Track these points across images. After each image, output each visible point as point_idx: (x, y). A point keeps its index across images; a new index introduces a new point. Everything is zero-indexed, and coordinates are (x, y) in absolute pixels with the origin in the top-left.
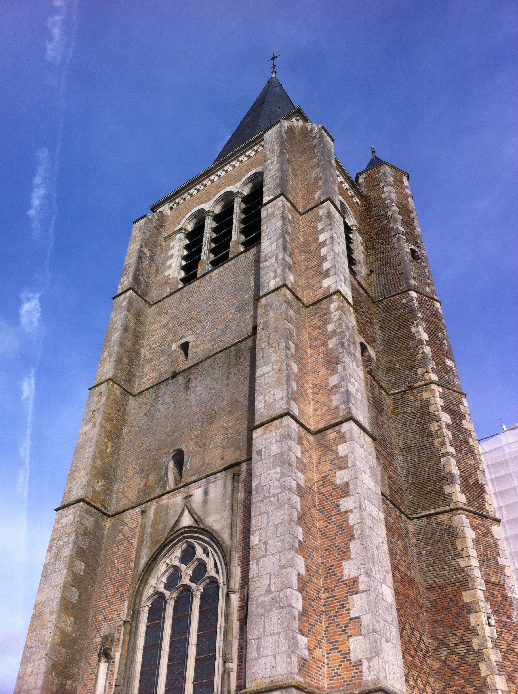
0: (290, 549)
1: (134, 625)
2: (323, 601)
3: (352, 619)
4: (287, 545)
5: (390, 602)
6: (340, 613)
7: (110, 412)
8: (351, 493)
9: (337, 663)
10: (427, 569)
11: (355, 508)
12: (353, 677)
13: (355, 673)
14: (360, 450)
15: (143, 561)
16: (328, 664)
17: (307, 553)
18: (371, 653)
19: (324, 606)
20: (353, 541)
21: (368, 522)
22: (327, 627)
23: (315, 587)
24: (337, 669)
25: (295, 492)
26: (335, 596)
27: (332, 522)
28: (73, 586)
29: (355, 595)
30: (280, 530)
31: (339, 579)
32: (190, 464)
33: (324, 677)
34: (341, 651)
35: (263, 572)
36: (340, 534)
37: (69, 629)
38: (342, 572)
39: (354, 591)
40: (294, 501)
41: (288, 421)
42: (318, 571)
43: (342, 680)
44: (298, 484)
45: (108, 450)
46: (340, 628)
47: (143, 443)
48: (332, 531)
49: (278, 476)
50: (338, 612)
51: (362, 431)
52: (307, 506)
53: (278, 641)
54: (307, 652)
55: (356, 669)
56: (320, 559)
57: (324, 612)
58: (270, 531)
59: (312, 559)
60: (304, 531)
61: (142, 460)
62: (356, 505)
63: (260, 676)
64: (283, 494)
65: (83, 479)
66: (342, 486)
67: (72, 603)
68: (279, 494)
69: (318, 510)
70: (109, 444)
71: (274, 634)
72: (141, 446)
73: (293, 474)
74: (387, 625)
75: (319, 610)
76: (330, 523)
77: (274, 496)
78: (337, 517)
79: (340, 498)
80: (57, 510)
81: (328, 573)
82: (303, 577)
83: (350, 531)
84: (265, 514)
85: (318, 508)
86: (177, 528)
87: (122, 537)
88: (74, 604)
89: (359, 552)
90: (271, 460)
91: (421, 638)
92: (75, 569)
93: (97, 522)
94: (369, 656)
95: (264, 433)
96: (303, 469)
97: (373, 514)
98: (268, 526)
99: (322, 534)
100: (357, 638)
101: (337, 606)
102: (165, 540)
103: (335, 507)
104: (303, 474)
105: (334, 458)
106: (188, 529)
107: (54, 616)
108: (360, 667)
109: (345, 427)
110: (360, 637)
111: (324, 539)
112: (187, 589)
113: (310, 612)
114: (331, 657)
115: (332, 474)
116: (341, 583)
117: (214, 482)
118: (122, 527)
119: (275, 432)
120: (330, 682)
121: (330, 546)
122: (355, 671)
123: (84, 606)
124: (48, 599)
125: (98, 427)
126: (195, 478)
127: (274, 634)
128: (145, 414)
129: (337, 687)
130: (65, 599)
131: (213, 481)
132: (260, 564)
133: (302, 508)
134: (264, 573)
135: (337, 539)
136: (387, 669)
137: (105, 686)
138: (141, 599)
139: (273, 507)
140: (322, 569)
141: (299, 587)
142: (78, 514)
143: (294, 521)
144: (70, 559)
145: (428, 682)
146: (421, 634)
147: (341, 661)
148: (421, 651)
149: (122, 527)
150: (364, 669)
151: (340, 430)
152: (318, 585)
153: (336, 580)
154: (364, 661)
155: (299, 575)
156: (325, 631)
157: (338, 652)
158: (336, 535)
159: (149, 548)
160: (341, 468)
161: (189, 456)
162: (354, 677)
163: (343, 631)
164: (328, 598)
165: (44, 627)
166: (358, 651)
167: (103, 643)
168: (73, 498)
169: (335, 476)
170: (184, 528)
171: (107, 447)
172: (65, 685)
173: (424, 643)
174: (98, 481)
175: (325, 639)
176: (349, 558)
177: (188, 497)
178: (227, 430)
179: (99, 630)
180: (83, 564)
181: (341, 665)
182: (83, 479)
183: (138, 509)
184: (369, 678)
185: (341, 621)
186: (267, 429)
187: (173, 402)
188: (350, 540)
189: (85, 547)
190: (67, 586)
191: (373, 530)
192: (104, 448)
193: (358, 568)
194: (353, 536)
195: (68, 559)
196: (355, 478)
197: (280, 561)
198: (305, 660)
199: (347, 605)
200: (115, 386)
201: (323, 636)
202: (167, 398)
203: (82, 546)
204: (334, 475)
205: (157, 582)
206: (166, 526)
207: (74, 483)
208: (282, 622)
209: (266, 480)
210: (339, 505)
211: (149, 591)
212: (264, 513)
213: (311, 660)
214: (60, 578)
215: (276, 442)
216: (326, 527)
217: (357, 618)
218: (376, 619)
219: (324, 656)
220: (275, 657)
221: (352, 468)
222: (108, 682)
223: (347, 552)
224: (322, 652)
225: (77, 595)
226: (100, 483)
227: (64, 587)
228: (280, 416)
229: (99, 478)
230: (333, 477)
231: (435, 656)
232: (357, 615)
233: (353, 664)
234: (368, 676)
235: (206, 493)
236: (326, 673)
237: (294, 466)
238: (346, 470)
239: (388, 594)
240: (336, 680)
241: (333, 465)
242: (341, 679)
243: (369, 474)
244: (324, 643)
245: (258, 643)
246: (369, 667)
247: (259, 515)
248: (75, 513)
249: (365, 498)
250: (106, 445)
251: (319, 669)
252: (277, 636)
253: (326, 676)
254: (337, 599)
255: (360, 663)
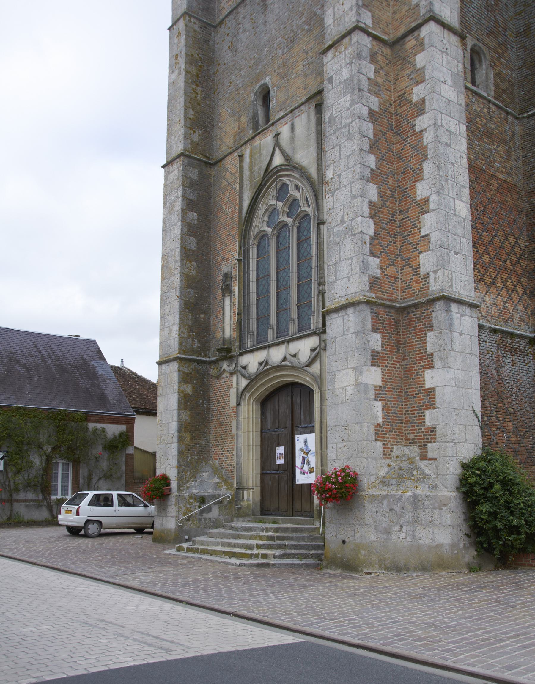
0: (361, 179)
1: (246, 262)
2: (398, 223)
3: (423, 237)
4: (357, 176)
5: (464, 216)
6: (413, 232)
7: (193, 53)
8: (426, 110)
9: (409, 277)
10: (531, 172)
11: (430, 126)
12: (421, 288)
13: (423, 285)
14: (440, 57)
15: (246, 204)
16: (401, 279)
17: (380, 179)
18: (437, 266)
19: (399, 227)
20: (426, 161)
21: (445, 139)
22: (401, 246)
23: (389, 211)
24: (409, 283)
25: (366, 119)
26: (408, 217)
27: (408, 144)
28: (190, 236)
29: (426, 215)
30: (352, 162)
31: (413, 201)
32: (276, 99)
33: (398, 290)
34: (412, 267)
35: (338, 204)
36: (415, 156)
37: (194, 273)
38: (415, 193)
39: (425, 211)
40: (365, 129)
41: (356, 37)
42: (394, 195)
43: (413, 292)
44: (370, 109)
45: (199, 97)
46: (412, 246)
47: (231, 83)
48: (408, 153)
49: (348, 104)
50: (411, 231)
51: (446, 31)
52: (381, 131)
53: (351, 265)
54: (379, 271)
55: (424, 281)
56: (396, 183)
57: (399, 233)
58: (342, 164)
59: (386, 184)
60: (377, 158)
61: (232, 102)
62: (431, 122)
63: (338, 296)
64: (354, 123)
65: (180, 133)
66: (418, 103)
67: (191, 250)
68: (350, 123)
69: (395, 133)
70: (199, 89)
71: (348, 259)
72: (230, 86)
73: (364, 99)
74: (458, 238)
75: (394, 232)
76: (406, 145)
77: (345, 126)
78: (412, 138)
79: (416, 117)
80: (163, 167)
81: (403, 196)
82: (375, 203)
83: (424, 151)
84: (338, 147)
85: (395, 131)
86: (271, 168)
87: (226, 183)
88: (194, 251)
89: (431, 172)
90: (342, 87)
91: (516, 242)
92: (189, 220)
93: (201, 173)
94: (435, 269)
95: (335, 56)
96: (377, 91)
97: (452, 129)
98: (340, 159)
99: (398, 157)
100: (426, 253)
101: (410, 226)
102: (262, 182)
103: (411, 128)
104: (377, 97)
105: (412, 72)
106: (279, 169)
107: (178, 264)
108: (428, 279)
109: (424, 31)
110: (429, 253)
111: (400, 162)
112: (284, 225)
113: (384, 235)
114: (404, 272)
115: (409, 91)
116: (414, 204)
117: (299, 115)
118: (224, 174)
119: (345, 53)
120: (402, 294)
121: (406, 168)
122: (424, 283)
123: (203, 251)
124: (171, 251)
125: (183, 73)
126: (282, 114)
127: (348, 259)
128: (229, 47)
129: (408, 297)
130: (185, 248)
131: (298, 114)
132: (335, 197)
133: (375, 135)
134: (339, 205)
135: (412, 161)
136: (454, 278)
137: (231, 315)
138: (249, 239)
139: (344, 139)
140: (398, 192)
141: (370, 214)
142: (181, 168)
143: (365, 151)
144: (182, 212)
145: (519, 282)
146: (517, 239)
147: (412, 276)
148: (515, 254)
149: (224, 174)
150: (431, 280)
151: (419, 35)
152: (393, 209)
153: (410, 202)
154: (431, 273)
155: (371, 202)
156: (400, 250)
157: (410, 267)
158: (411, 158)
159: (250, 191)
160: (418, 83)
161: (274, 90)
162: (423, 288)
163: (414, 248)
164: (403, 219)
165: (172, 274)
166: (427, 265)
167: (224, 281)
168: (174, 154)
169: (412, 92)
170: (276, 167)
171: (197, 94)
172: (199, 318)
173: (520, 247)
174: (194, 132)
175: (399, 257)
176: (423, 179)
177: (277, 135)
178: (307, 54)
179: (220, 269)
180: (195, 214)
181: (412, 279)
182: (180, 133)
183: (236, 154)
184: (434, 288)
185: (413, 240)
186: (336, 51)
187: (253, 28)
188: (424, 161)
189: (194, 198)
190: (184, 236)
191: (450, 146)
192: (194, 95)
193: (430, 188)
194: (427, 156)
195: (180, 212)
196: (431, 92)
197: (351, 192)
198: (378, 278)
199: (419, 225)
200: (193, 20)
201: (397, 255)
202: (247, 25)
203: (191, 198)
204: (411, 91)
205: (260, 224)
206: (261, 167)
207: (173, 137)
208: (354, 247)
209: (338, 110)
210: (415, 125)
211: (254, 231)
212: (337, 145)
213: (383, 277)
214: (177, 231)
215: (346, 66)
216: (402, 150)
217: (427, 235)
218: (444, 235)
219: (398, 272)
220: (349, 279)
221: (429, 81)
222: (232, 312)
223: (421, 173)
224: (396, 269)
225: (195, 242)
226: (197, 134)
227: (182, 237)
228: (349, 33)
229: (195, 128)
230: (410, 94)
231: (531, 258)
232: (427, 233)
233: (422, 277)
234: (434, 286)
235: (293, 128)
236: (400, 286)
237: (366, 90)
238: (423, 84)
239: (463, 209)
240: (408, 292)
241: (411, 79)
242: (412, 290)
243: (450, 84)
244: (398, 261)
245: (336, 268)
246: (435, 278)
247: (333, 148)
248: (178, 168)
249: (441, 113)
250: (195, 92)
251: (392, 284)
252: (350, 261)
253: (400, 289)
254: (410, 220)
255: (427, 276)
